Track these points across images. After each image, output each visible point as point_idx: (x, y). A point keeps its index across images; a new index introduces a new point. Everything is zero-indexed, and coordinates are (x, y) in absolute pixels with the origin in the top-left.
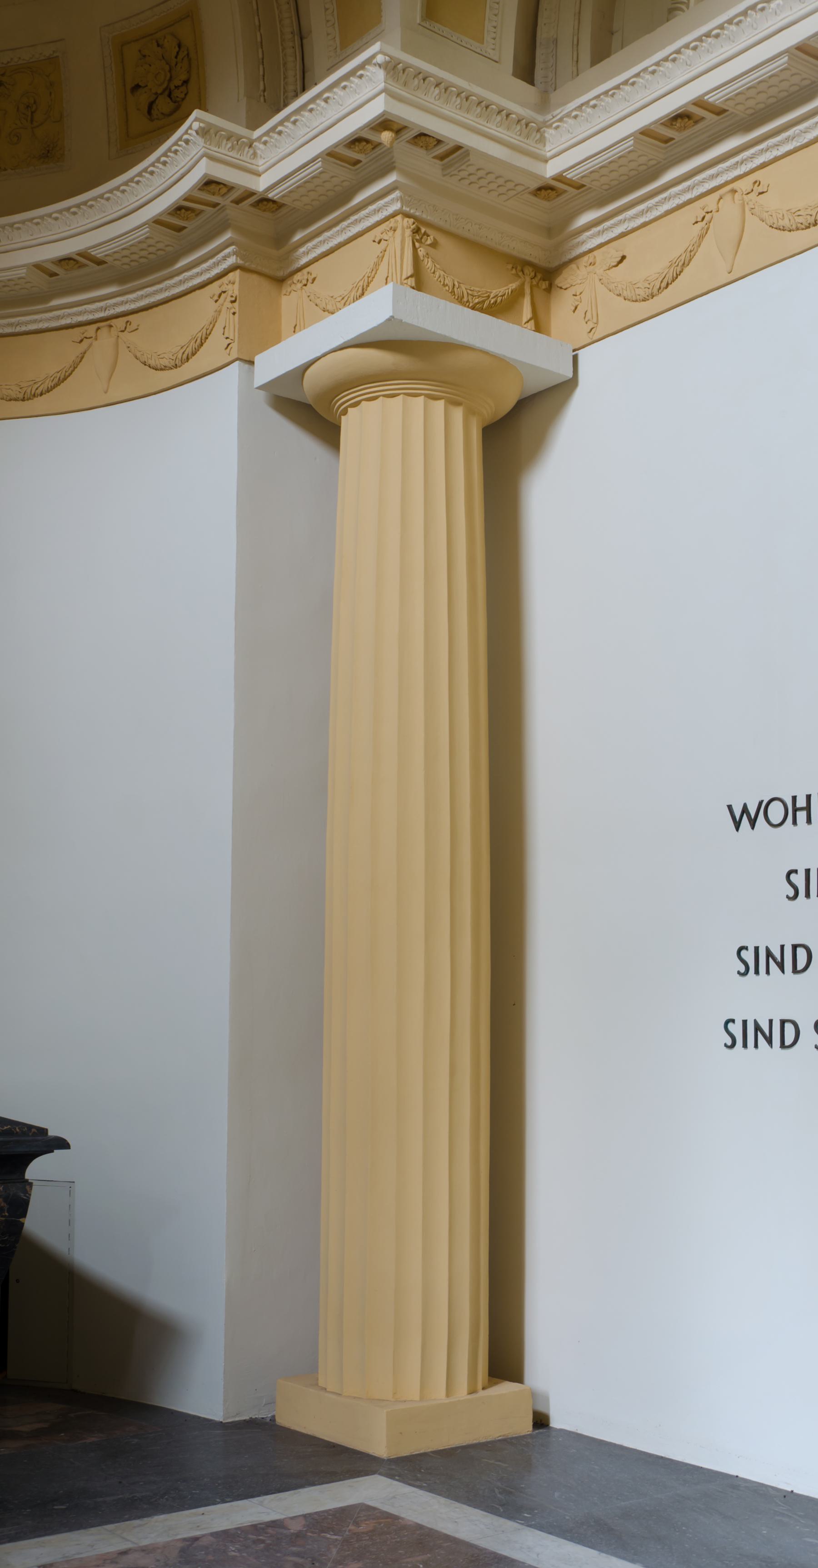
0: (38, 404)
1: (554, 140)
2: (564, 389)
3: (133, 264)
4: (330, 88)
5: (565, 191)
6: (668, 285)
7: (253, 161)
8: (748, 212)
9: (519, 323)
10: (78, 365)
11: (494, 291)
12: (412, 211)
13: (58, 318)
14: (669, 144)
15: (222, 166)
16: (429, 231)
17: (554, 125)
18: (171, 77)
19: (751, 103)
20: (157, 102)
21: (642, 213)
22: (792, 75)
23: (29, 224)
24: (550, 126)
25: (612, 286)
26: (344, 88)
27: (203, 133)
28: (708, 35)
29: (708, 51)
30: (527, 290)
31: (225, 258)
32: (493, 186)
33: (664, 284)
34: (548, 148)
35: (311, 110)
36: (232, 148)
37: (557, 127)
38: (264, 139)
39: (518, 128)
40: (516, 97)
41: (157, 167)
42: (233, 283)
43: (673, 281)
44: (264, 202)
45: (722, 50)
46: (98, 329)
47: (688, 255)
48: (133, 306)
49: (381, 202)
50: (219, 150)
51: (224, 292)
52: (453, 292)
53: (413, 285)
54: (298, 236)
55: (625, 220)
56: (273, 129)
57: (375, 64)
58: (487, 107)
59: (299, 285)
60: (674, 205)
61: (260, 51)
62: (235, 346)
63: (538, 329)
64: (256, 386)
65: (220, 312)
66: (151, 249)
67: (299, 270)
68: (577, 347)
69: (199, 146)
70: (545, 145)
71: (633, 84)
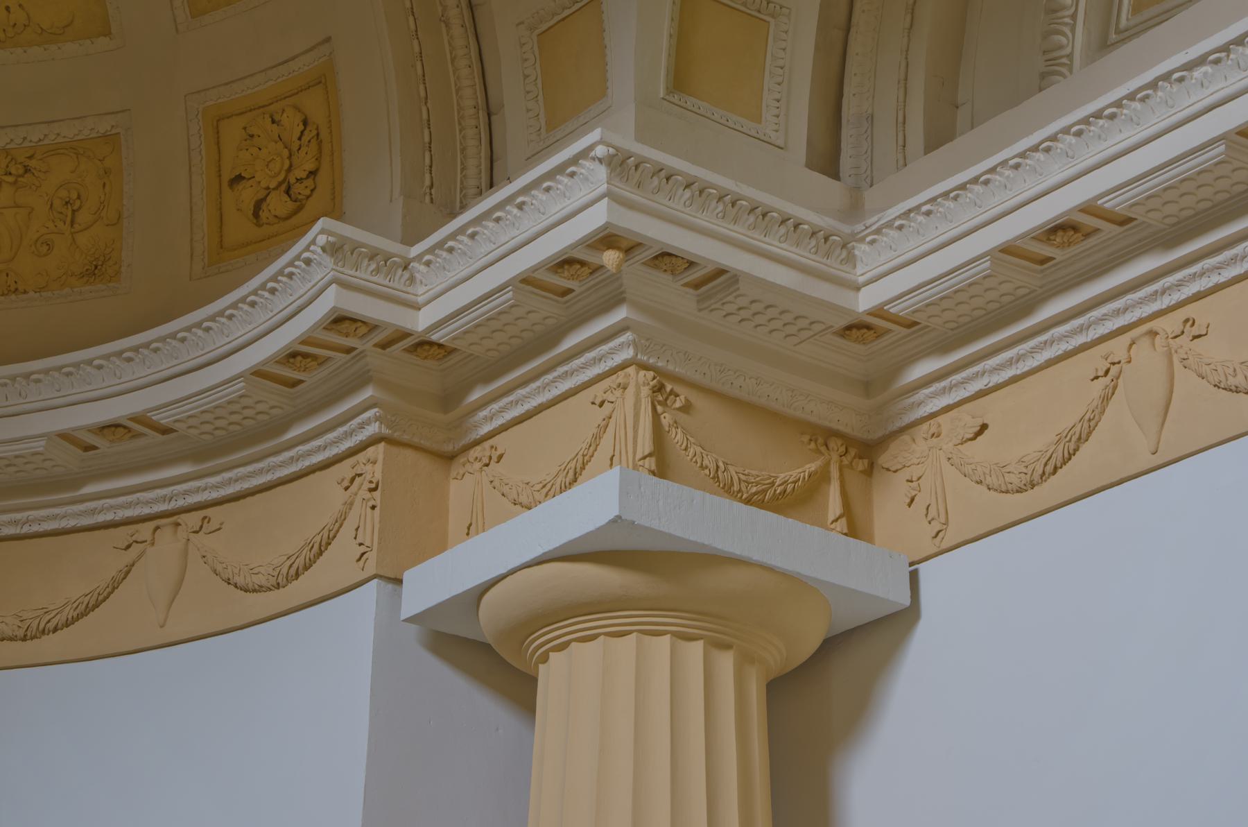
0: (49, 645)
1: (868, 260)
2: (899, 622)
3: (218, 433)
4: (526, 190)
5: (888, 331)
6: (1055, 469)
7: (409, 289)
8: (1177, 365)
9: (823, 525)
10: (119, 584)
11: (782, 475)
12: (651, 361)
13: (93, 512)
14: (1046, 266)
15: (361, 297)
16: (678, 389)
17: (868, 239)
18: (291, 166)
19: (1171, 209)
20: (269, 199)
21: (1010, 363)
22: (1234, 170)
23: (56, 374)
24: (862, 240)
25: (968, 469)
26: (548, 189)
27: (334, 250)
28: (1098, 115)
29: (1100, 137)
30: (835, 473)
31: (362, 426)
32: (777, 324)
33: (1049, 468)
34: (859, 271)
35: (498, 220)
36: (377, 271)
37: (873, 242)
38: (427, 257)
39: (813, 242)
40: (810, 200)
41: (262, 297)
42: (374, 463)
43: (1064, 463)
44: (423, 345)
45: (1122, 136)
46: (157, 528)
47: (1086, 425)
48: (215, 495)
49: (605, 348)
50: (357, 274)
51: (360, 475)
52: (716, 478)
53: (653, 467)
54: (476, 395)
55: (984, 372)
56: (440, 245)
57: (593, 159)
58: (764, 215)
59: (478, 465)
60: (1060, 352)
61: (426, 132)
62: (372, 556)
63: (854, 531)
64: (403, 618)
65: (352, 504)
66: (247, 412)
67: (477, 443)
68: (916, 559)
69: (325, 268)
70: (855, 267)
71: (986, 182)
